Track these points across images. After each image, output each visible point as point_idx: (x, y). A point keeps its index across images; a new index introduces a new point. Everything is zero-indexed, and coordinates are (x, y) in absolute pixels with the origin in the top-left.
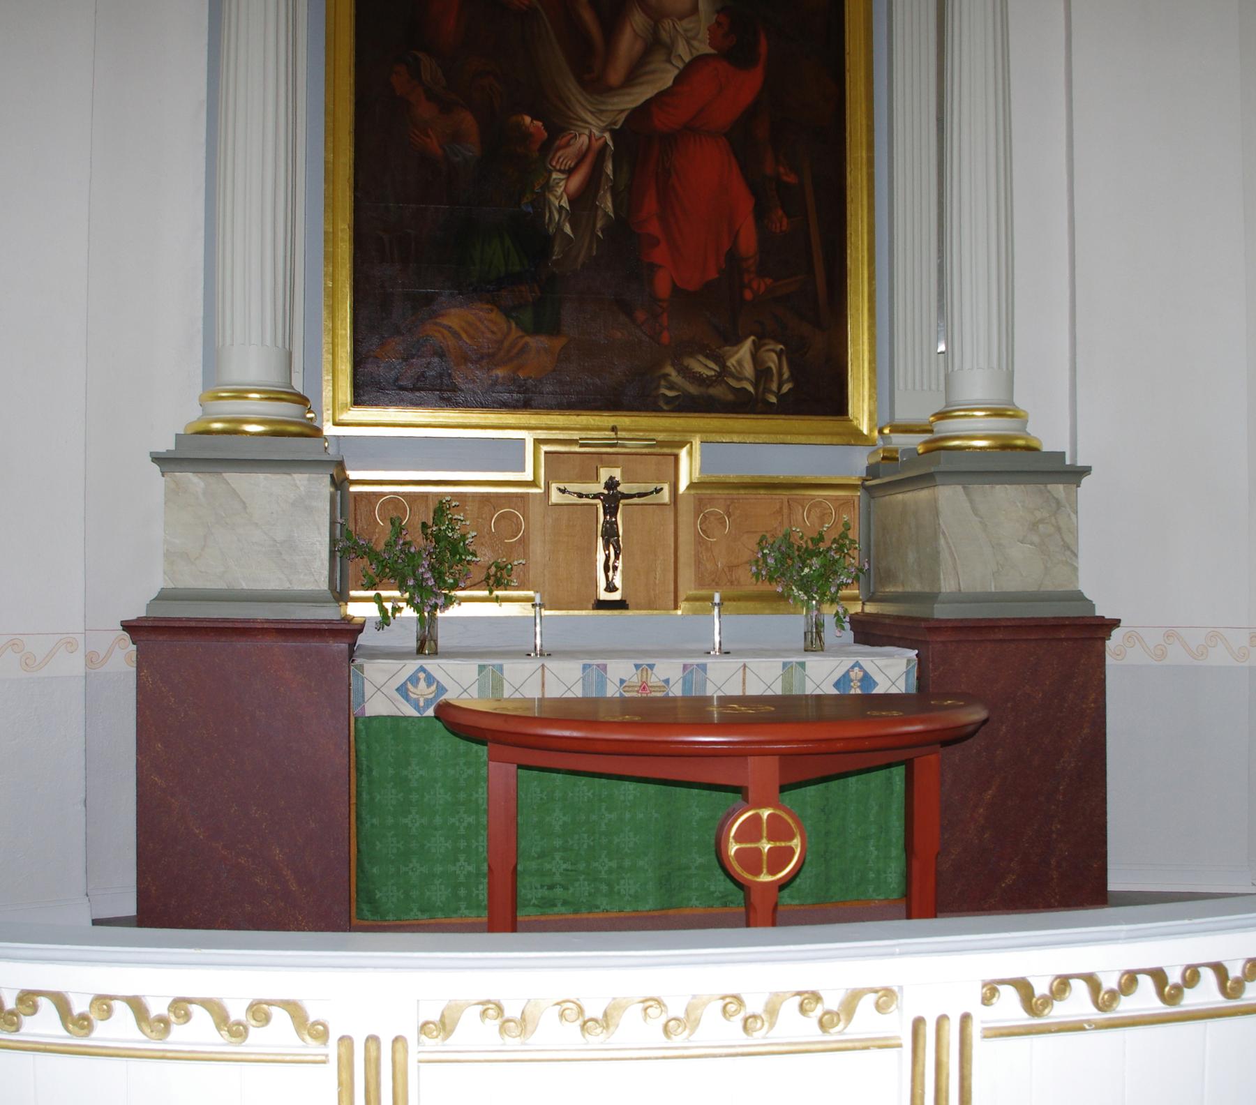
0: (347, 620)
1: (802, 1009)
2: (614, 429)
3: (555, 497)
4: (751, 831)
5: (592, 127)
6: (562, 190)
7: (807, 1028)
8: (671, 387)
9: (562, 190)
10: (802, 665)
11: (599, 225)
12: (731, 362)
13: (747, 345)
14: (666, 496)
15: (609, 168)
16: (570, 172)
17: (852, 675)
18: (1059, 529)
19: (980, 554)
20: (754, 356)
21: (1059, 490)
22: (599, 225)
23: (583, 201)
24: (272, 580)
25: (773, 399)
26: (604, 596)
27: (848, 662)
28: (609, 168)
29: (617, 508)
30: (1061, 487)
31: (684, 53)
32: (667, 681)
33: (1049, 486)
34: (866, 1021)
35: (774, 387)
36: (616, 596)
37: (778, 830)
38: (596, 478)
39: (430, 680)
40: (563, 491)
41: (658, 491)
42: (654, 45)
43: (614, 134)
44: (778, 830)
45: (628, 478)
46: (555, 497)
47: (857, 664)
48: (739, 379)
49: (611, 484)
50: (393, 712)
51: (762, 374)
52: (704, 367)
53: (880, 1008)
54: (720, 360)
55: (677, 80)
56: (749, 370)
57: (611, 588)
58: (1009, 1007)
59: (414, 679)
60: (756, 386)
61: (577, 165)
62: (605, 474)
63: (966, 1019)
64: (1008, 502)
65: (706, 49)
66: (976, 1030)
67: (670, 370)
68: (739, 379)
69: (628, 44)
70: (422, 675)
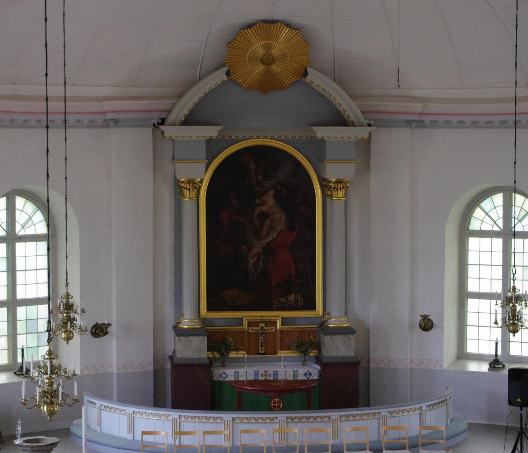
3: (250, 331)
4: (275, 402)
5: (258, 248)
6: (251, 262)
7: (269, 421)
8: (276, 305)
9: (251, 262)
11: (260, 269)
12: (289, 299)
13: (293, 295)
14: (274, 330)
15: (262, 256)
16: (253, 258)
18: (350, 344)
19: (336, 348)
20: (294, 297)
22: (260, 269)
23: (256, 264)
24: (197, 356)
25: (299, 307)
26: (260, 352)
28: (262, 256)
31: (278, 229)
35: (299, 304)
36: (263, 352)
37: (279, 402)
38: (258, 326)
39: (225, 374)
41: (272, 329)
42: (272, 228)
43: (263, 249)
44: (279, 402)
45: (265, 326)
46: (250, 331)
48: (291, 302)
51: (296, 301)
52: (283, 300)
54: (287, 299)
55: (277, 235)
56: (293, 300)
59: (222, 374)
60: (295, 304)
61: (255, 256)
62: (261, 325)
64: (339, 339)
65: (283, 228)
67: (275, 301)
68: (291, 302)
69: (266, 228)
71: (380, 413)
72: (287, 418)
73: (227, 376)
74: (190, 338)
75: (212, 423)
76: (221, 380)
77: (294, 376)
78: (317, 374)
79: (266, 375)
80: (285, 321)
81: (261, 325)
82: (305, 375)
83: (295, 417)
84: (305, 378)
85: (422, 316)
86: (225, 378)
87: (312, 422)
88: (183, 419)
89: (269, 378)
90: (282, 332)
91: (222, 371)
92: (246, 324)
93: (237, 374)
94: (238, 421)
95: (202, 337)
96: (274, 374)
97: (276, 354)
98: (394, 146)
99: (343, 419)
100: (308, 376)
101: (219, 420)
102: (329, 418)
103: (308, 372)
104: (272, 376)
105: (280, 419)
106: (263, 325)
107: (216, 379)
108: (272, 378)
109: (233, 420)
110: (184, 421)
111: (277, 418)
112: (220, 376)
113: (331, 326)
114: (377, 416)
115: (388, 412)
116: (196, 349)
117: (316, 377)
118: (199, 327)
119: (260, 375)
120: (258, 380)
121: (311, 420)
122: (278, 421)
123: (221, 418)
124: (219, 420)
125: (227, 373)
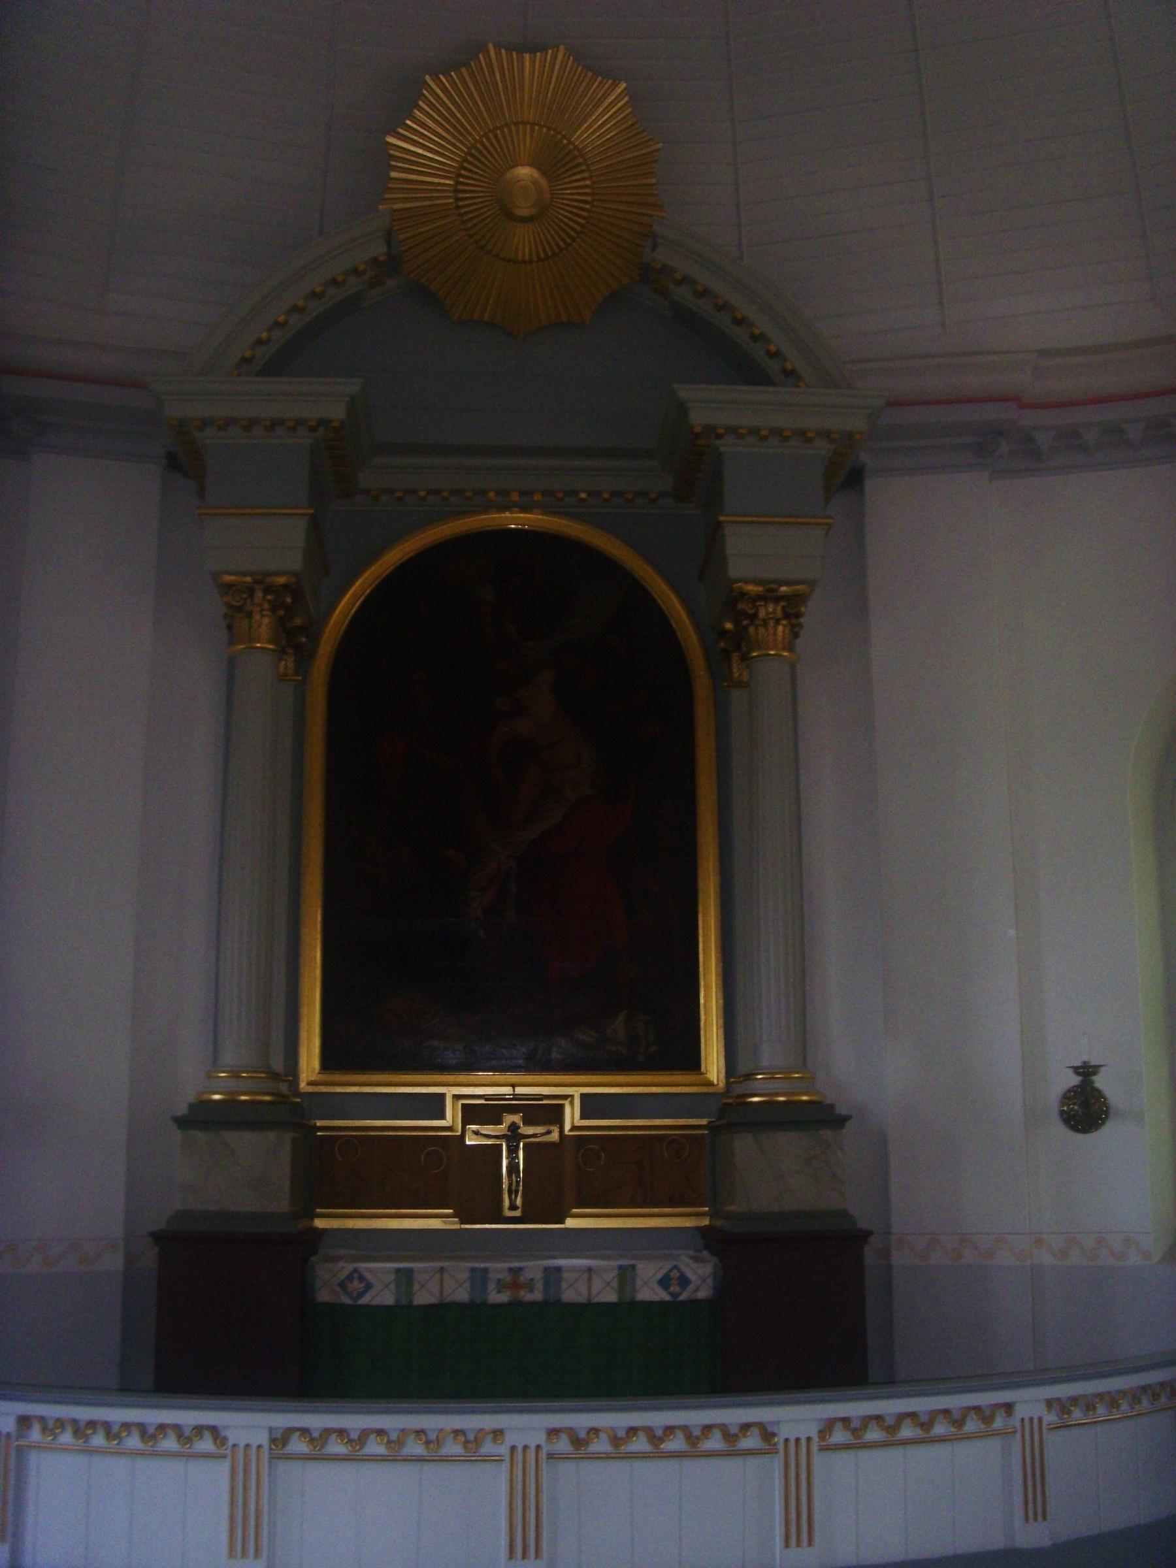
0: (316, 1230)
1: (455, 1438)
2: (513, 1086)
10: (633, 1267)
17: (672, 1274)
19: (774, 1180)
21: (828, 1134)
25: (641, 1058)
26: (508, 1213)
27: (668, 1265)
29: (518, 1146)
30: (829, 1132)
32: (532, 1280)
33: (821, 1132)
34: (488, 1447)
36: (518, 1213)
39: (362, 1279)
40: (476, 1133)
41: (549, 1132)
47: (675, 1267)
49: (513, 1127)
50: (656, 1298)
53: (495, 1439)
57: (513, 1207)
58: (563, 1445)
59: (350, 1278)
63: (538, 1447)
64: (788, 1146)
66: (543, 1454)
70: (356, 1275)
71: (1009, 1407)
72: (553, 1433)
73: (369, 1287)
74: (230, 1136)
75: (168, 1454)
76: (347, 1300)
77: (622, 1288)
78: (710, 1281)
79: (516, 1285)
80: (590, 1106)
81: (509, 1119)
82: (664, 1282)
83: (595, 1431)
84: (663, 1295)
85: (1076, 1070)
86: (361, 1295)
87: (680, 1455)
88: (35, 1434)
89: (527, 1296)
90: (580, 1142)
91: (350, 1267)
92: (452, 1116)
93: (405, 1278)
94: (298, 1445)
95: (271, 1135)
96: (547, 1283)
97: (563, 1223)
98: (923, 518)
99: (839, 1436)
100: (675, 1288)
101: (206, 1445)
102: (768, 1435)
103: (675, 1274)
104: (539, 1285)
105: (518, 1439)
106: (516, 1118)
107: (324, 1296)
108: (537, 1296)
109: (273, 1441)
110: (37, 1447)
111: (498, 1434)
112: (342, 1285)
113: (756, 1099)
114: (998, 1423)
115: (1049, 1403)
116: (249, 1178)
117: (702, 1294)
118: (267, 1098)
119: (491, 1286)
120: (484, 1304)
121: (676, 1443)
122: (504, 1450)
123: (214, 1430)
124: (206, 1445)
125: (367, 1275)
